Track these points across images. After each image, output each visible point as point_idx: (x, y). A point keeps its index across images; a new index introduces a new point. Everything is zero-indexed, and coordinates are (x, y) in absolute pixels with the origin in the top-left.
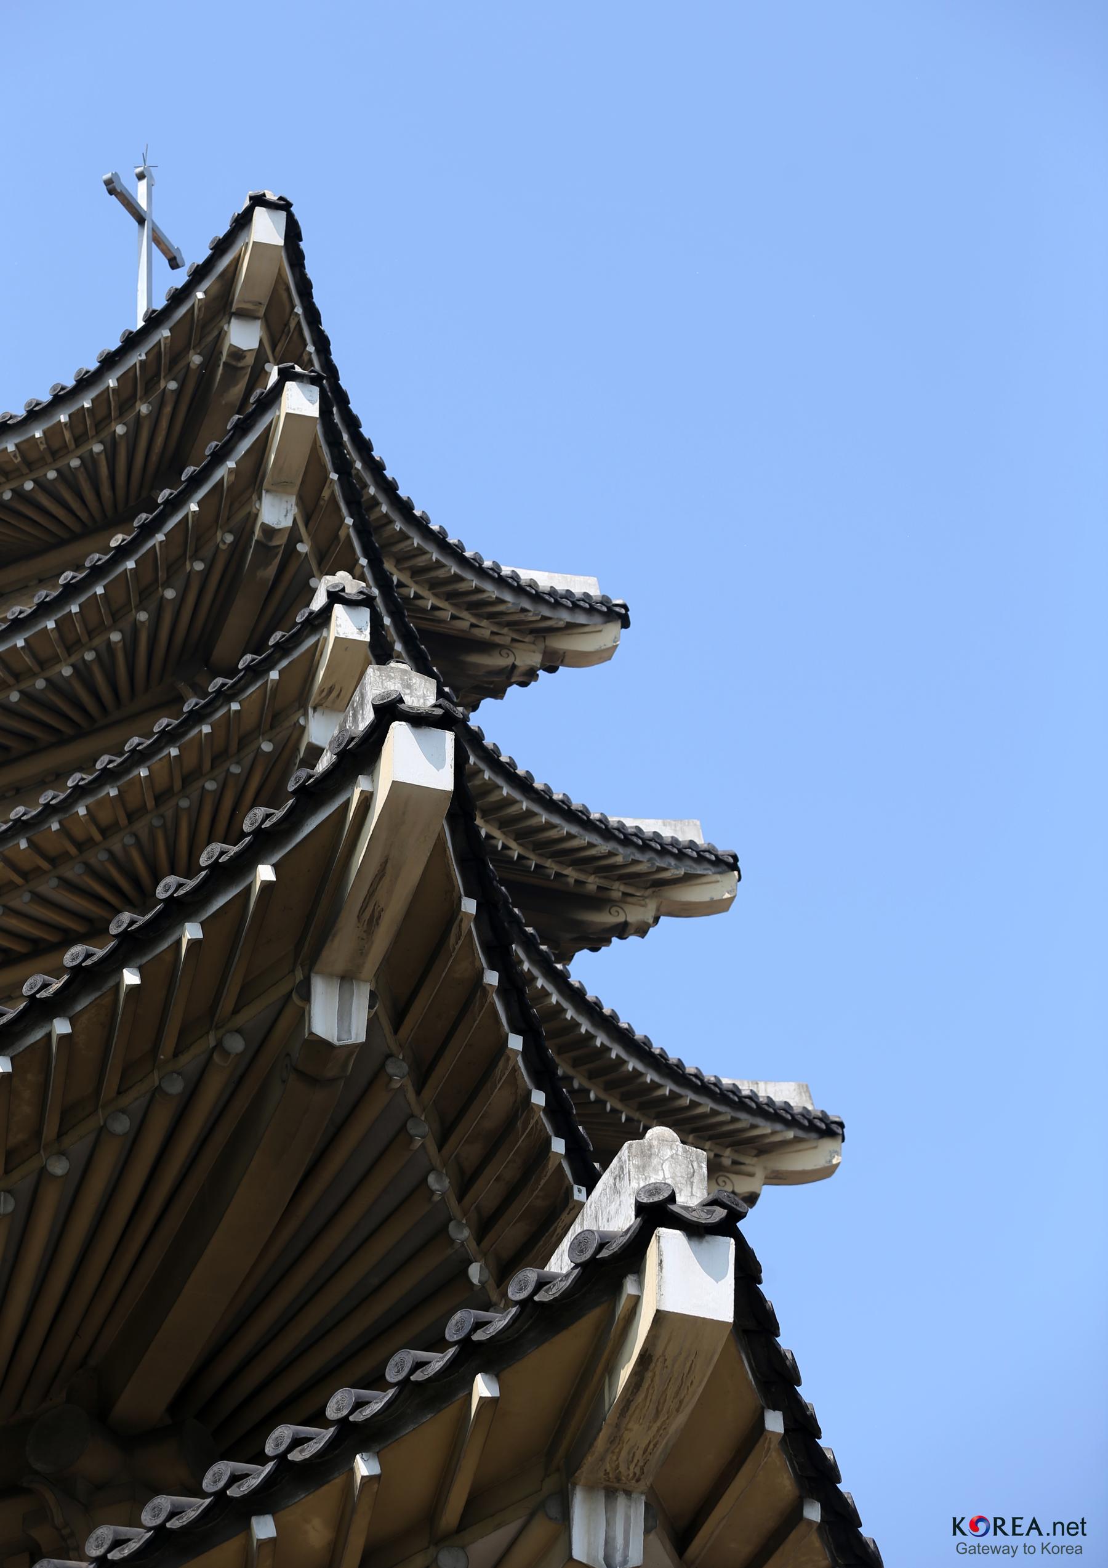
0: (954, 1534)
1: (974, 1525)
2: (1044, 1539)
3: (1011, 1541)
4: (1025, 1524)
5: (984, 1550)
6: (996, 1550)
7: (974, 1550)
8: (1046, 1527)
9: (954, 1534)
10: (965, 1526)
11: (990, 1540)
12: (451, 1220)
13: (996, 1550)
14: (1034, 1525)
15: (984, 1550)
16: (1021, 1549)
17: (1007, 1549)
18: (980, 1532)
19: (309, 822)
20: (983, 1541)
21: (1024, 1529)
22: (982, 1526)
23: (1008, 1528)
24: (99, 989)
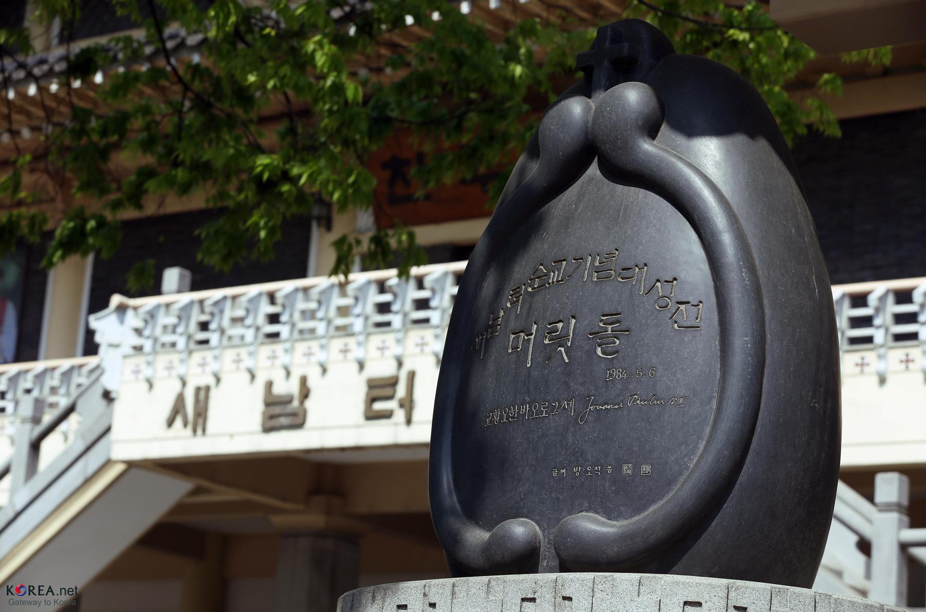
0: (170, 423)
1: (18, 590)
2: (55, 597)
3: (38, 598)
4: (45, 589)
5: (24, 603)
6: (30, 603)
7: (18, 603)
8: (56, 590)
9: (170, 423)
10: (13, 590)
11: (27, 597)
12: (565, 260)
13: (30, 603)
14: (50, 590)
15: (24, 603)
16: (43, 602)
17: (36, 603)
18: (22, 593)
19: (595, 532)
20: (23, 598)
21: (44, 592)
22: (22, 590)
23: (36, 591)
24: (97, 44)
